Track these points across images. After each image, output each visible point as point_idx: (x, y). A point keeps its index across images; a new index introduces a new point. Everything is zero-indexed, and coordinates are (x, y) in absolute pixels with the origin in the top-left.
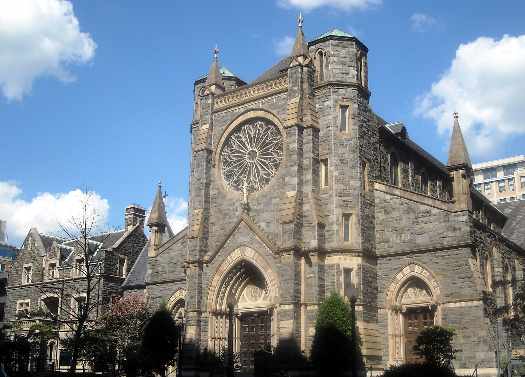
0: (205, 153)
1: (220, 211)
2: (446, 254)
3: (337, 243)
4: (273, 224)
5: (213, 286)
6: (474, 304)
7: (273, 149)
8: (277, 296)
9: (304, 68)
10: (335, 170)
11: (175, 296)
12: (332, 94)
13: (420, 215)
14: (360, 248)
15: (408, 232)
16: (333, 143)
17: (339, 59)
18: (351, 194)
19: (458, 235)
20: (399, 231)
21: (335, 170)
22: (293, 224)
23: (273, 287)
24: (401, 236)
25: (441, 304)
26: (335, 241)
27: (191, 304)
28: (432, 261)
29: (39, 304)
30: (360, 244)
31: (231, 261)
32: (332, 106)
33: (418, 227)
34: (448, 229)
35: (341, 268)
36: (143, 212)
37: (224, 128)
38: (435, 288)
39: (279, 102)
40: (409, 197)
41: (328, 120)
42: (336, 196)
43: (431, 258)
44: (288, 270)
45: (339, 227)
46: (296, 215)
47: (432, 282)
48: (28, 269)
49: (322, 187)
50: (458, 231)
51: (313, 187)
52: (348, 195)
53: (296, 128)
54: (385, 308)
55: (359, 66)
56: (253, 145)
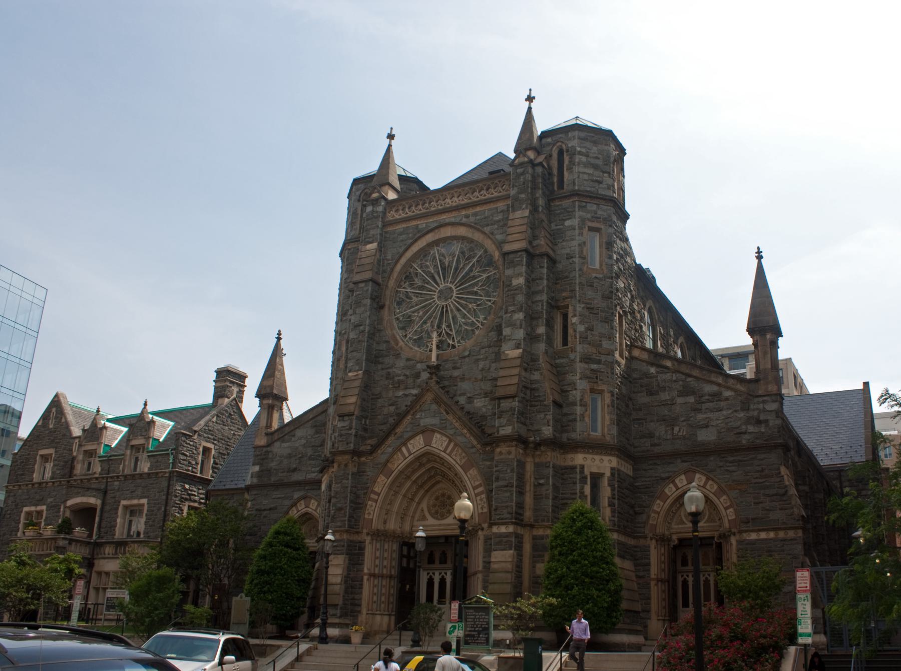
0: (370, 287)
1: (389, 376)
2: (746, 459)
3: (581, 433)
4: (478, 400)
5: (376, 493)
6: (788, 536)
7: (481, 286)
8: (485, 513)
9: (536, 168)
10: (580, 323)
11: (297, 508)
12: (577, 209)
13: (704, 399)
14: (614, 443)
15: (685, 423)
16: (577, 282)
17: (589, 159)
18: (603, 360)
19: (763, 430)
20: (671, 422)
21: (580, 323)
22: (517, 399)
23: (478, 498)
24: (673, 429)
25: (737, 534)
26: (578, 430)
27: (338, 519)
28: (722, 468)
29: (61, 513)
30: (614, 437)
31: (407, 455)
32: (577, 227)
33: (700, 416)
34: (748, 421)
35: (587, 472)
36: (242, 377)
37: (401, 250)
38: (726, 509)
39: (495, 215)
40: (688, 371)
41: (570, 247)
42: (581, 361)
43: (721, 464)
44: (506, 470)
45: (583, 409)
46: (521, 387)
47: (722, 500)
48: (45, 458)
49: (557, 347)
50: (763, 425)
51: (546, 346)
52: (599, 362)
53: (524, 255)
54: (645, 537)
55: (404, 225)
56: (448, 278)
